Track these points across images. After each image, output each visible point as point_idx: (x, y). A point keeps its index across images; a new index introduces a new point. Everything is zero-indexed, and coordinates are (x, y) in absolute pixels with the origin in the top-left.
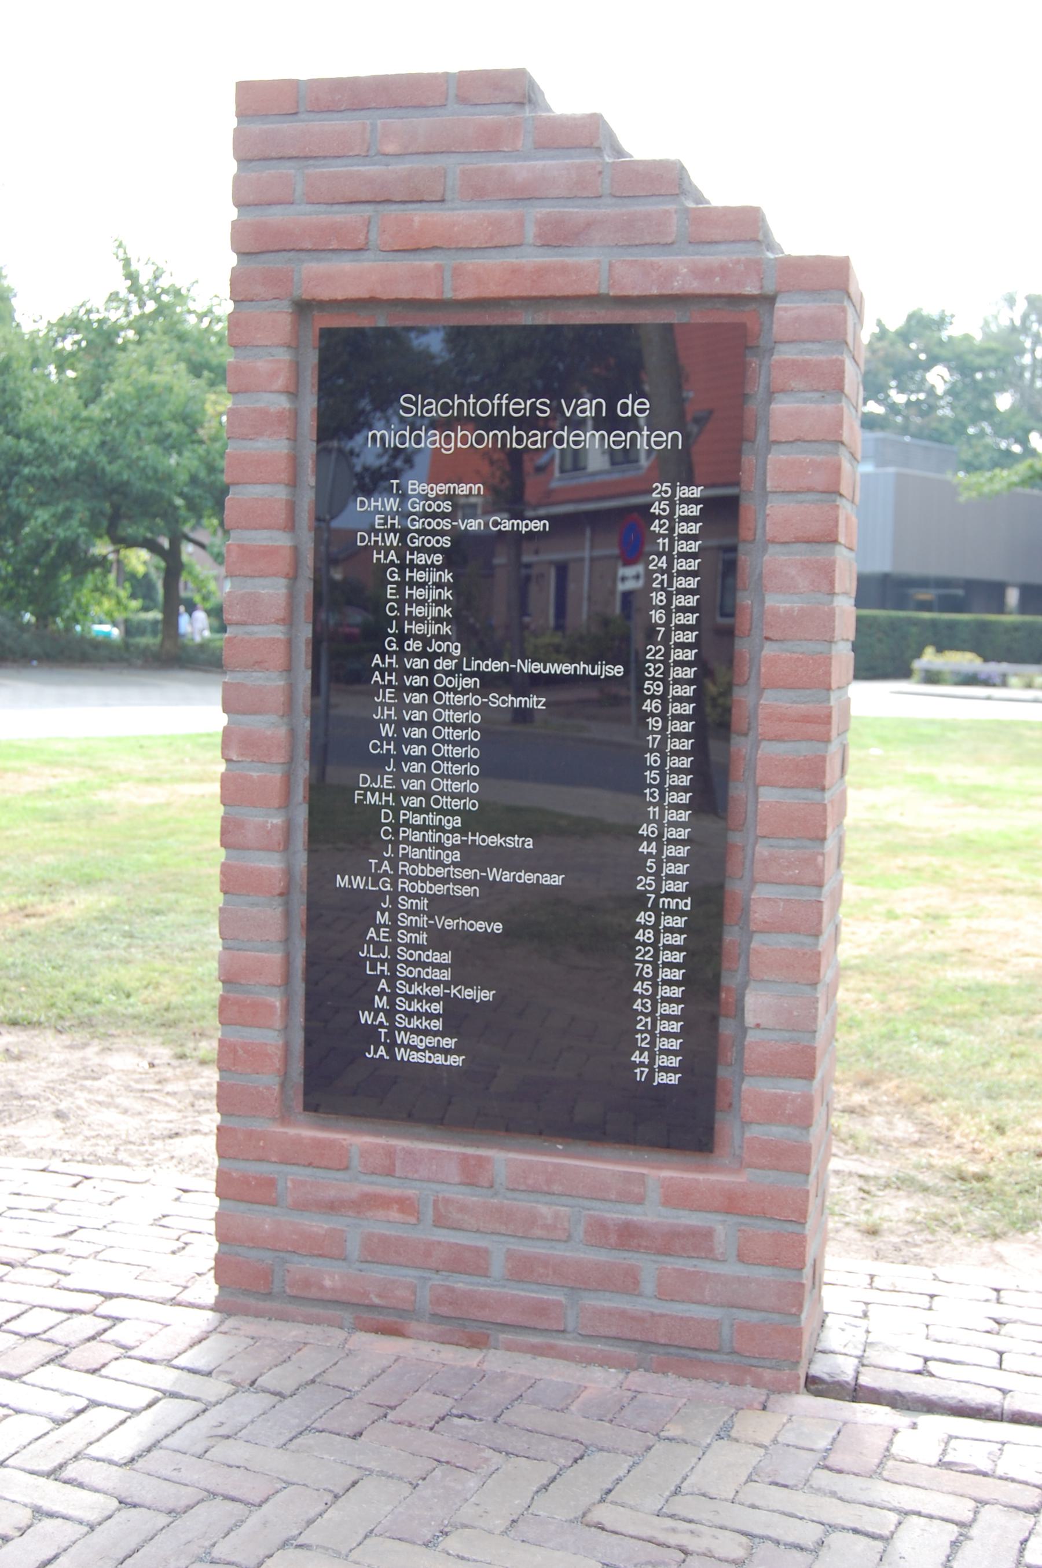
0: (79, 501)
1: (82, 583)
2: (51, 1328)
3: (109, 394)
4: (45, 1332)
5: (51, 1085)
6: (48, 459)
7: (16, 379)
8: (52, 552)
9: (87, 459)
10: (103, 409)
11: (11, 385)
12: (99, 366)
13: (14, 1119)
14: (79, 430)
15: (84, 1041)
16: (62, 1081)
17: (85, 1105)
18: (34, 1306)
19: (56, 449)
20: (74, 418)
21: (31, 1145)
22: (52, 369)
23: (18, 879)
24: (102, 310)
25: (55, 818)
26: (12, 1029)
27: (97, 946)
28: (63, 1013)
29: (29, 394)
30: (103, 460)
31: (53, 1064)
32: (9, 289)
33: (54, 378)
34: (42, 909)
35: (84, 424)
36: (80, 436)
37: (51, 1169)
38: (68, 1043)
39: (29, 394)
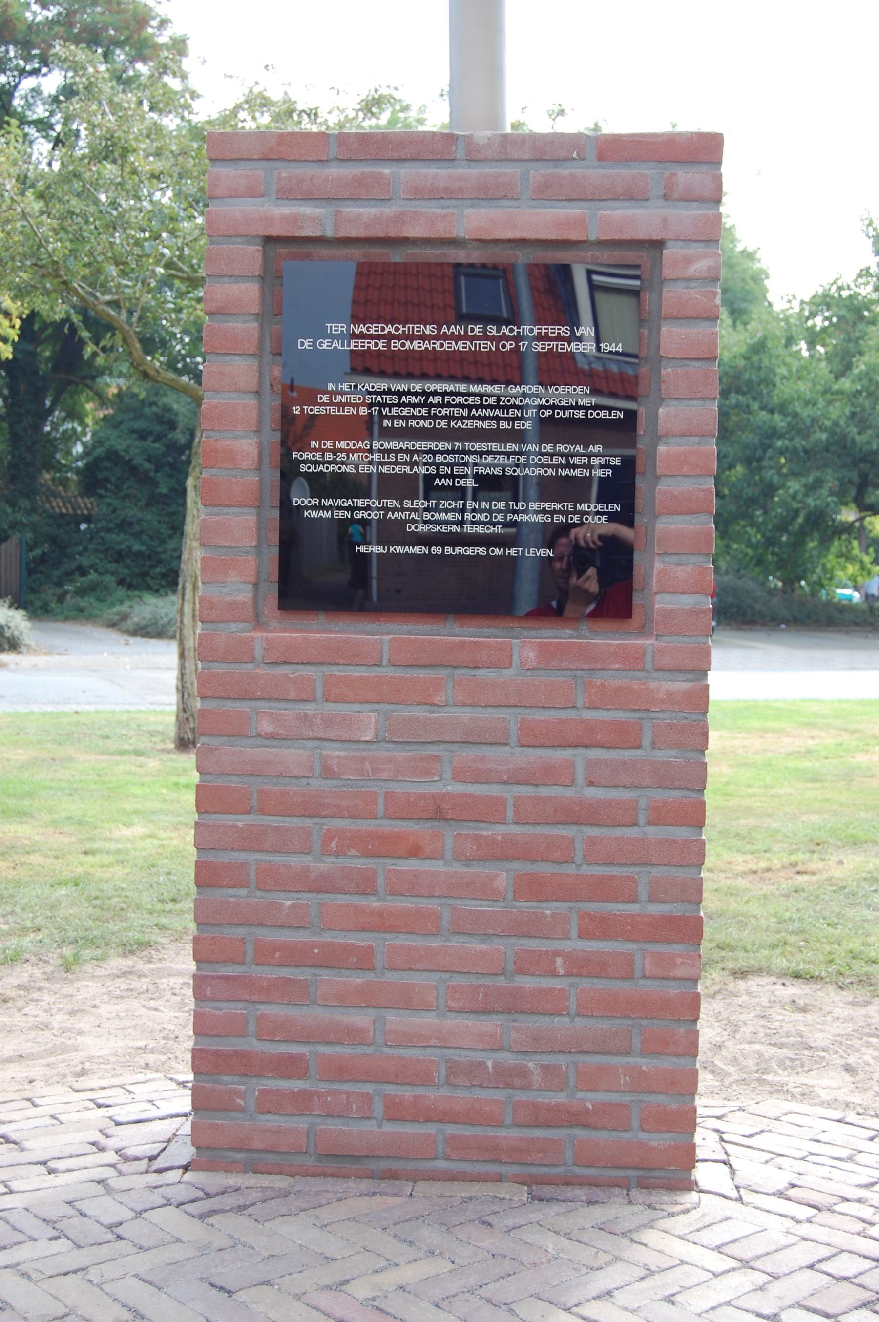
0: (829, 471)
1: (828, 549)
2: (861, 1274)
3: (860, 367)
4: (855, 1277)
5: (838, 1038)
6: (800, 432)
7: (771, 356)
8: (800, 520)
9: (838, 430)
10: (853, 382)
11: (766, 362)
12: (849, 340)
13: (806, 1068)
14: (830, 403)
15: (866, 998)
16: (849, 1036)
17: (872, 1062)
18: (843, 1251)
19: (808, 422)
20: (825, 392)
21: (825, 1095)
22: (803, 345)
23: (787, 837)
24: (852, 286)
25: (816, 778)
26: (795, 981)
27: (868, 906)
28: (842, 969)
29: (783, 371)
30: (853, 430)
31: (838, 1018)
32: (762, 271)
33: (805, 353)
34: (812, 867)
35: (834, 397)
36: (831, 408)
37: (847, 1120)
38: (851, 999)
39: (783, 371)
